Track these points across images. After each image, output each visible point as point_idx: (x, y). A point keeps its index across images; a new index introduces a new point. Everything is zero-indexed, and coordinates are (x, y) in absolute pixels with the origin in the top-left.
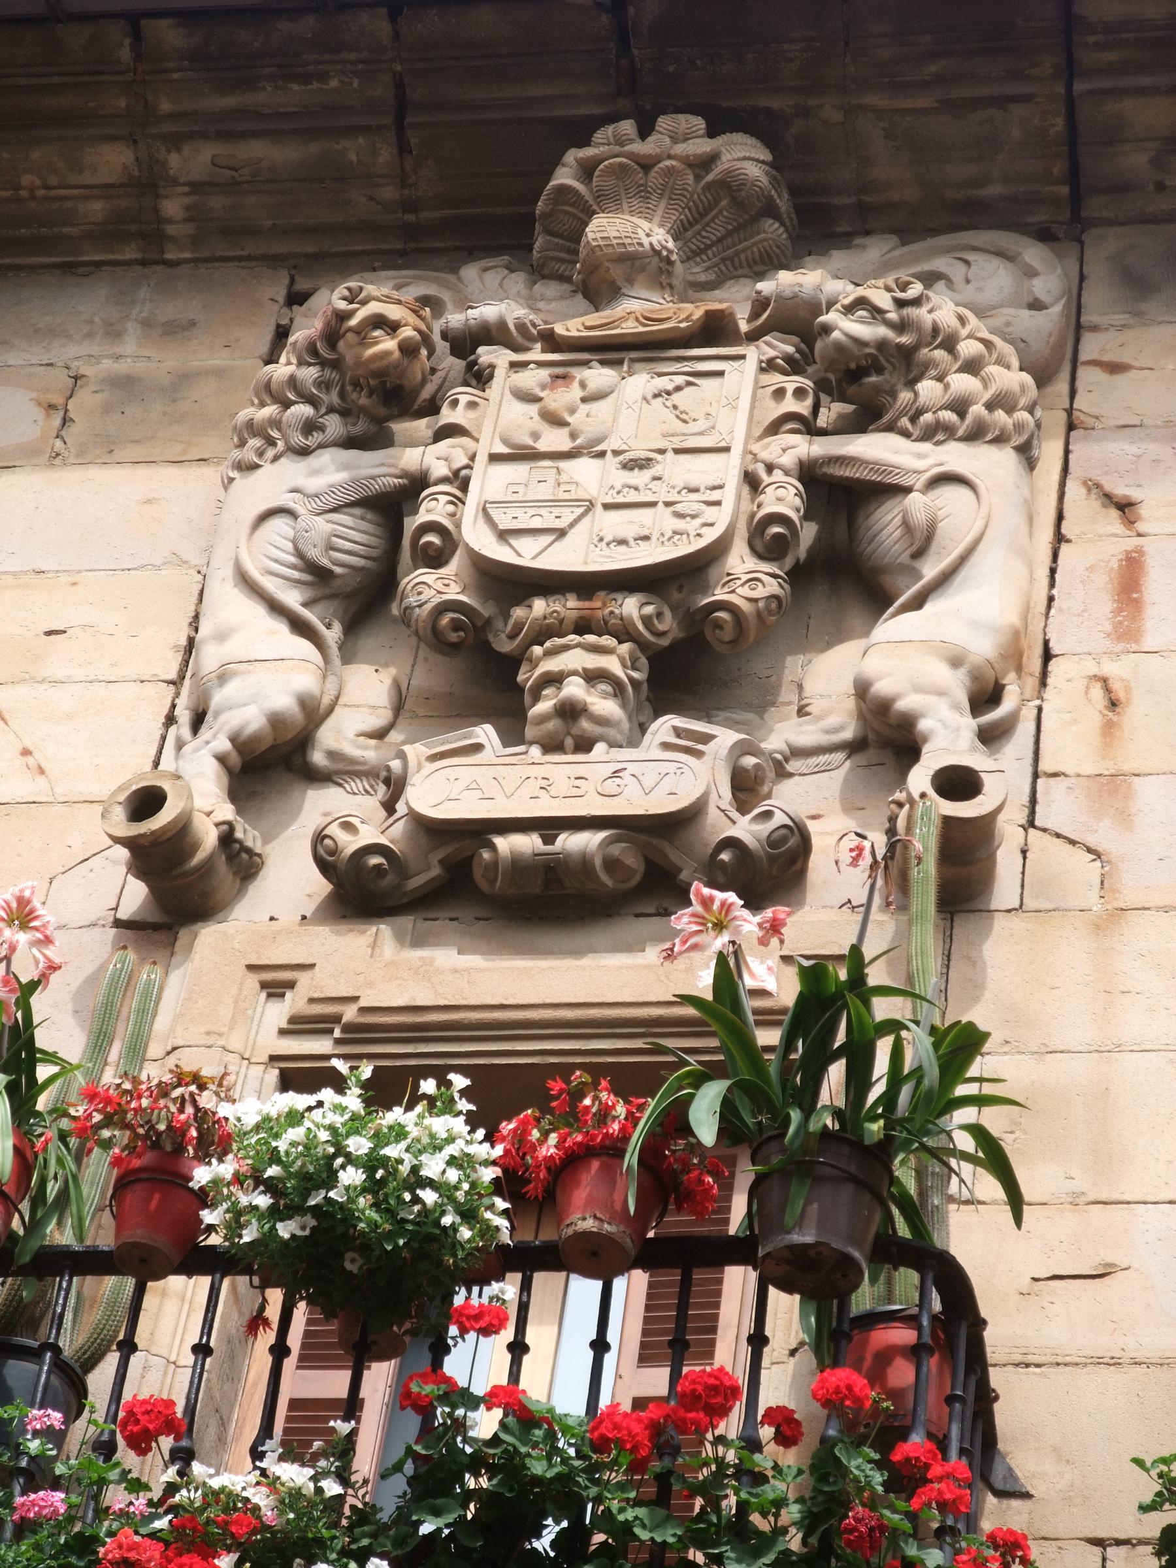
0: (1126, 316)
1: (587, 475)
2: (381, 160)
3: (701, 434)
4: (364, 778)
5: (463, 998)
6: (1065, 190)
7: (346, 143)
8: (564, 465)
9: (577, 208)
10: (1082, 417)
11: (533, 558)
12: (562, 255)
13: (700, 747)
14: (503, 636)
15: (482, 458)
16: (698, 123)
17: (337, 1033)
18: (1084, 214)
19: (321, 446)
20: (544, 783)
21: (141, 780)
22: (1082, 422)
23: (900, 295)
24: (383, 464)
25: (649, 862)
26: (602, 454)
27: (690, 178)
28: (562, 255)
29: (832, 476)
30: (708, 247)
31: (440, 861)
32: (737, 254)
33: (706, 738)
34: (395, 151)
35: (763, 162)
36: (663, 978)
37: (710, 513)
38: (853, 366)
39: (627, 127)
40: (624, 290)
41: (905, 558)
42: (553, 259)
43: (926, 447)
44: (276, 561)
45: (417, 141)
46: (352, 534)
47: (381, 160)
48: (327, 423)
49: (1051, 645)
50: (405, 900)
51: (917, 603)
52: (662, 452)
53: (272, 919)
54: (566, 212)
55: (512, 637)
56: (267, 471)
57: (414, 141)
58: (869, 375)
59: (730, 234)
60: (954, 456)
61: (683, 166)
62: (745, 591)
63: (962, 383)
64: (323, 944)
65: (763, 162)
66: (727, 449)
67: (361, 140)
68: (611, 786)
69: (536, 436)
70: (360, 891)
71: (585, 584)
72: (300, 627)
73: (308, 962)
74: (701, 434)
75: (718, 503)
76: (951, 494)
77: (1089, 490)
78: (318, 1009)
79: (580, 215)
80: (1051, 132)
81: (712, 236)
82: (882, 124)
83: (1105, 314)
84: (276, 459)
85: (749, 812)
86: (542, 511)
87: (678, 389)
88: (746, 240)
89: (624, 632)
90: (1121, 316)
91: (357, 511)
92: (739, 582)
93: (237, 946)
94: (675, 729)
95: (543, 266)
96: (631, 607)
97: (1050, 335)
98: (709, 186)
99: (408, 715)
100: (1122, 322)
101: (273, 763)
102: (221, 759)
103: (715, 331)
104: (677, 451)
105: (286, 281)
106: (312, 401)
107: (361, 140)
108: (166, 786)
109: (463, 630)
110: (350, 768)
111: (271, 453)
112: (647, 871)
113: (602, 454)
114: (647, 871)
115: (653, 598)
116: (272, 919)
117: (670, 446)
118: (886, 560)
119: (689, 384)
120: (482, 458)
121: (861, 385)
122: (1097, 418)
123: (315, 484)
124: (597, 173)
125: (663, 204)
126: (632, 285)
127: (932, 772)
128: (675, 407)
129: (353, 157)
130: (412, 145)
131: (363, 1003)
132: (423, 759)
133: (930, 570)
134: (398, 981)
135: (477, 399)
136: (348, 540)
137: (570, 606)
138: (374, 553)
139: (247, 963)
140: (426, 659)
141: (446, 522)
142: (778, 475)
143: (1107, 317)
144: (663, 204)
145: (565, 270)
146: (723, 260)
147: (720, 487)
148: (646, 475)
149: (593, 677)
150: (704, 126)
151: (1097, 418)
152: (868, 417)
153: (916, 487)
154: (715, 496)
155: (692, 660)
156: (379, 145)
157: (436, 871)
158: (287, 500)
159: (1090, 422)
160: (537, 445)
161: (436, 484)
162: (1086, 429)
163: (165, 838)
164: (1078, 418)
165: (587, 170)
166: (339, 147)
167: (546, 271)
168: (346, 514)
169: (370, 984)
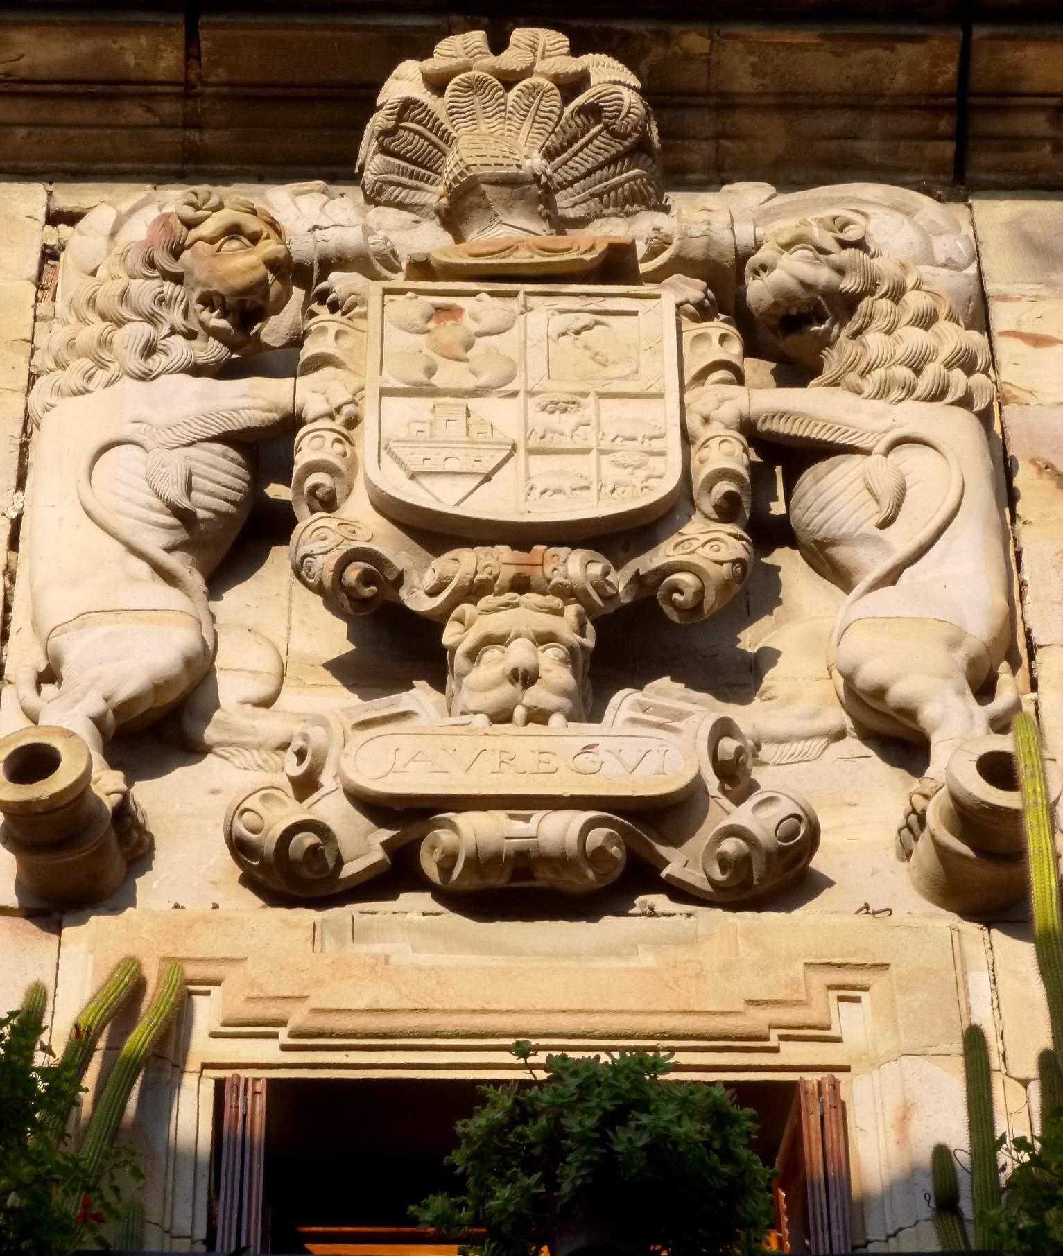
0: (1039, 286)
1: (502, 416)
2: (163, 64)
3: (624, 378)
4: (255, 752)
5: (435, 1001)
6: (949, 148)
7: (124, 42)
8: (473, 403)
9: (425, 126)
10: (1014, 392)
11: (457, 504)
12: (404, 180)
13: (675, 724)
14: (421, 594)
15: (371, 394)
16: (562, 41)
17: (284, 1038)
18: (968, 175)
19: (165, 372)
20: (505, 757)
21: (24, 736)
22: (1015, 397)
23: (842, 236)
24: (245, 396)
25: (631, 854)
26: (514, 394)
27: (557, 101)
28: (404, 180)
29: (777, 434)
30: (576, 180)
31: (385, 845)
32: (608, 191)
33: (680, 715)
34: (181, 55)
35: (634, 88)
36: (671, 984)
37: (655, 462)
38: (794, 311)
39: (477, 37)
40: (501, 217)
41: (870, 528)
42: (391, 183)
43: (879, 405)
44: (127, 499)
45: (210, 45)
46: (215, 474)
47: (163, 64)
48: (171, 346)
49: (1034, 634)
50: (339, 889)
51: (891, 577)
52: (584, 395)
53: (177, 906)
54: (411, 130)
55: (433, 593)
56: (99, 396)
57: (205, 45)
58: (811, 324)
59: (601, 166)
60: (913, 416)
61: (551, 85)
62: (707, 551)
63: (913, 338)
64: (252, 936)
65: (634, 88)
66: (660, 396)
67: (143, 40)
68: (584, 761)
69: (431, 371)
70: (290, 874)
71: (522, 536)
72: (169, 577)
73: (240, 955)
74: (624, 378)
75: (661, 454)
76: (909, 457)
77: (1040, 470)
78: (256, 1011)
79: (428, 134)
80: (940, 80)
81: (581, 168)
82: (753, 59)
83: (1015, 282)
84: (110, 383)
85: (468, 861)
86: (457, 453)
87: (587, 328)
88: (620, 174)
89: (568, 593)
90: (1032, 286)
91: (218, 447)
92: (695, 544)
93: (147, 936)
94: (641, 704)
95: (380, 192)
96: (576, 566)
97: (970, 300)
98: (582, 110)
99: (293, 683)
100: (1035, 293)
101: (160, 728)
102: (98, 721)
103: (616, 266)
104: (602, 395)
105: (44, 197)
106: (151, 319)
107: (143, 40)
108: (58, 743)
109: (374, 584)
110: (236, 739)
111: (102, 376)
112: (620, 863)
113: (514, 394)
114: (620, 863)
115: (600, 557)
116: (177, 906)
117: (593, 390)
118: (842, 532)
119: (597, 323)
120: (371, 394)
121: (792, 335)
122: (1031, 392)
123: (161, 416)
124: (450, 87)
125: (526, 126)
126: (510, 213)
127: (976, 758)
128: (586, 347)
129: (131, 60)
130: (203, 48)
131: (314, 1003)
132: (349, 727)
133: (902, 539)
134: (352, 981)
135: (347, 328)
136: (218, 480)
137: (499, 560)
138: (238, 496)
139: (162, 955)
140: (303, 622)
141: (337, 462)
142: (715, 428)
143: (1016, 286)
144: (526, 126)
145: (406, 197)
146: (592, 196)
147: (662, 436)
148: (570, 419)
149: (544, 639)
150: (568, 43)
151: (1031, 392)
152: (797, 371)
153: (876, 450)
154: (657, 445)
155: (633, 642)
156: (162, 47)
157: (378, 855)
158: (127, 431)
159: (1027, 397)
160: (434, 380)
161: (314, 420)
162: (1020, 404)
163: (63, 804)
164: (1009, 392)
165: (437, 84)
166: (116, 47)
167: (383, 198)
168: (205, 449)
169: (319, 983)
